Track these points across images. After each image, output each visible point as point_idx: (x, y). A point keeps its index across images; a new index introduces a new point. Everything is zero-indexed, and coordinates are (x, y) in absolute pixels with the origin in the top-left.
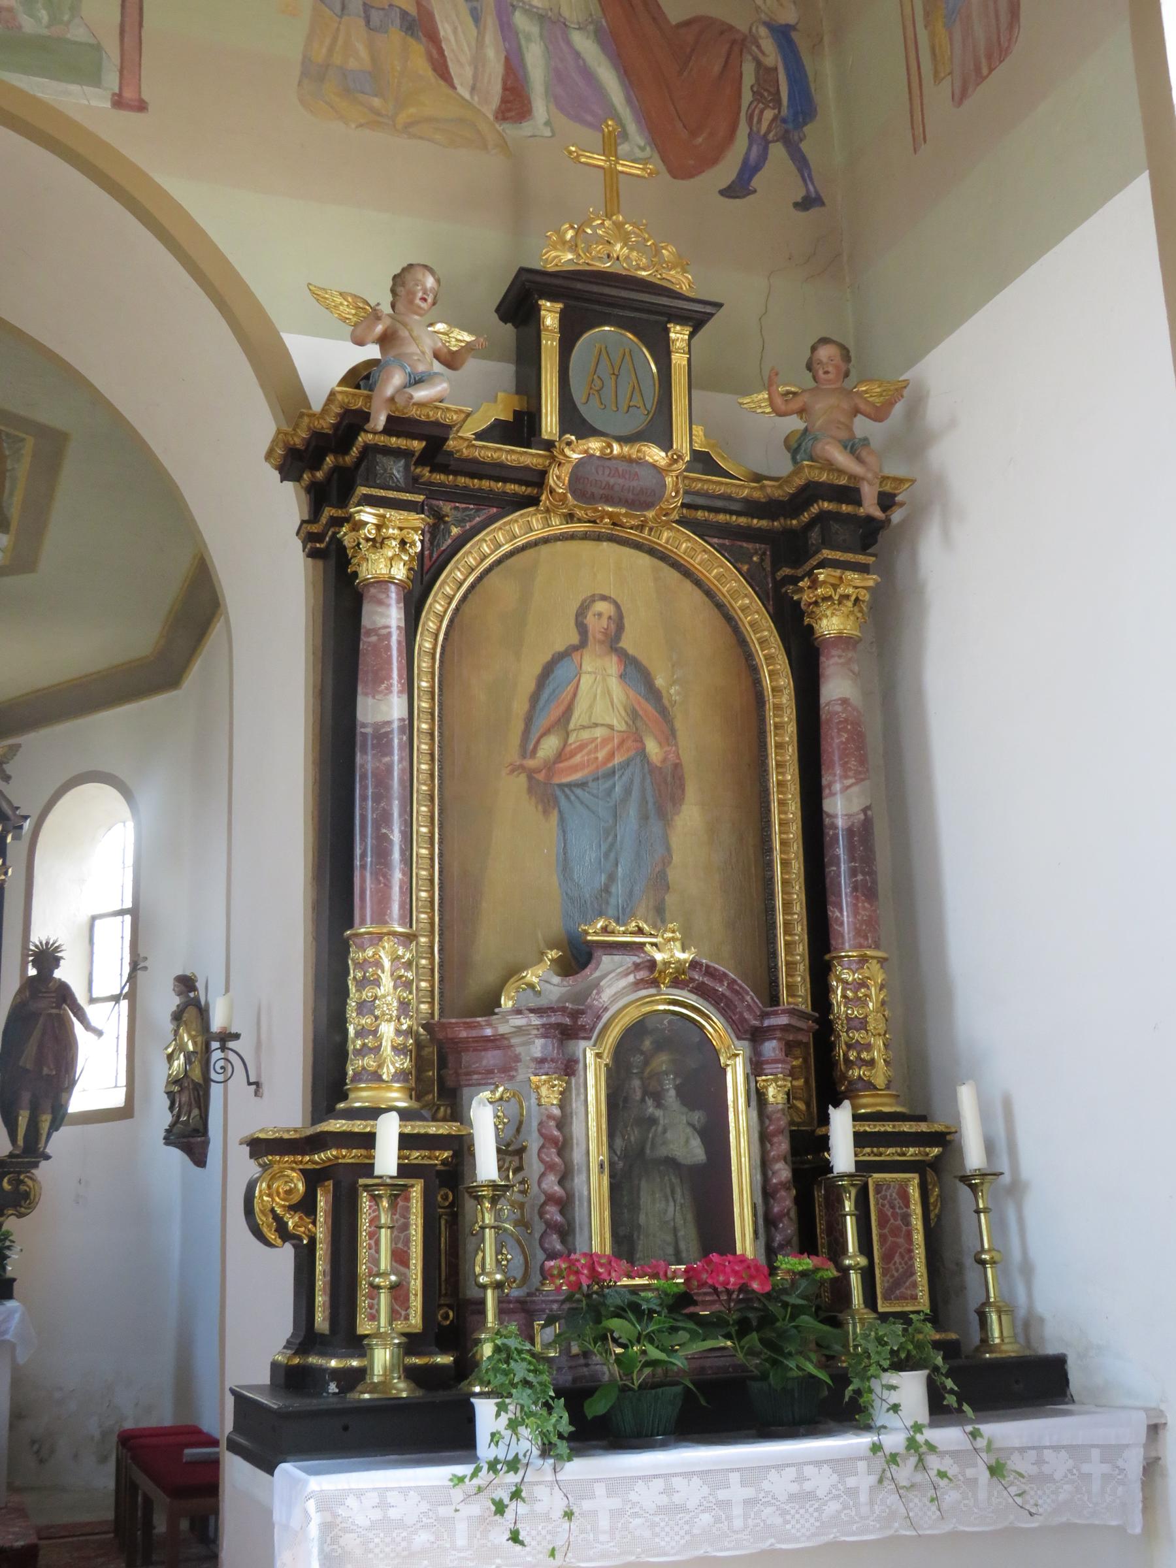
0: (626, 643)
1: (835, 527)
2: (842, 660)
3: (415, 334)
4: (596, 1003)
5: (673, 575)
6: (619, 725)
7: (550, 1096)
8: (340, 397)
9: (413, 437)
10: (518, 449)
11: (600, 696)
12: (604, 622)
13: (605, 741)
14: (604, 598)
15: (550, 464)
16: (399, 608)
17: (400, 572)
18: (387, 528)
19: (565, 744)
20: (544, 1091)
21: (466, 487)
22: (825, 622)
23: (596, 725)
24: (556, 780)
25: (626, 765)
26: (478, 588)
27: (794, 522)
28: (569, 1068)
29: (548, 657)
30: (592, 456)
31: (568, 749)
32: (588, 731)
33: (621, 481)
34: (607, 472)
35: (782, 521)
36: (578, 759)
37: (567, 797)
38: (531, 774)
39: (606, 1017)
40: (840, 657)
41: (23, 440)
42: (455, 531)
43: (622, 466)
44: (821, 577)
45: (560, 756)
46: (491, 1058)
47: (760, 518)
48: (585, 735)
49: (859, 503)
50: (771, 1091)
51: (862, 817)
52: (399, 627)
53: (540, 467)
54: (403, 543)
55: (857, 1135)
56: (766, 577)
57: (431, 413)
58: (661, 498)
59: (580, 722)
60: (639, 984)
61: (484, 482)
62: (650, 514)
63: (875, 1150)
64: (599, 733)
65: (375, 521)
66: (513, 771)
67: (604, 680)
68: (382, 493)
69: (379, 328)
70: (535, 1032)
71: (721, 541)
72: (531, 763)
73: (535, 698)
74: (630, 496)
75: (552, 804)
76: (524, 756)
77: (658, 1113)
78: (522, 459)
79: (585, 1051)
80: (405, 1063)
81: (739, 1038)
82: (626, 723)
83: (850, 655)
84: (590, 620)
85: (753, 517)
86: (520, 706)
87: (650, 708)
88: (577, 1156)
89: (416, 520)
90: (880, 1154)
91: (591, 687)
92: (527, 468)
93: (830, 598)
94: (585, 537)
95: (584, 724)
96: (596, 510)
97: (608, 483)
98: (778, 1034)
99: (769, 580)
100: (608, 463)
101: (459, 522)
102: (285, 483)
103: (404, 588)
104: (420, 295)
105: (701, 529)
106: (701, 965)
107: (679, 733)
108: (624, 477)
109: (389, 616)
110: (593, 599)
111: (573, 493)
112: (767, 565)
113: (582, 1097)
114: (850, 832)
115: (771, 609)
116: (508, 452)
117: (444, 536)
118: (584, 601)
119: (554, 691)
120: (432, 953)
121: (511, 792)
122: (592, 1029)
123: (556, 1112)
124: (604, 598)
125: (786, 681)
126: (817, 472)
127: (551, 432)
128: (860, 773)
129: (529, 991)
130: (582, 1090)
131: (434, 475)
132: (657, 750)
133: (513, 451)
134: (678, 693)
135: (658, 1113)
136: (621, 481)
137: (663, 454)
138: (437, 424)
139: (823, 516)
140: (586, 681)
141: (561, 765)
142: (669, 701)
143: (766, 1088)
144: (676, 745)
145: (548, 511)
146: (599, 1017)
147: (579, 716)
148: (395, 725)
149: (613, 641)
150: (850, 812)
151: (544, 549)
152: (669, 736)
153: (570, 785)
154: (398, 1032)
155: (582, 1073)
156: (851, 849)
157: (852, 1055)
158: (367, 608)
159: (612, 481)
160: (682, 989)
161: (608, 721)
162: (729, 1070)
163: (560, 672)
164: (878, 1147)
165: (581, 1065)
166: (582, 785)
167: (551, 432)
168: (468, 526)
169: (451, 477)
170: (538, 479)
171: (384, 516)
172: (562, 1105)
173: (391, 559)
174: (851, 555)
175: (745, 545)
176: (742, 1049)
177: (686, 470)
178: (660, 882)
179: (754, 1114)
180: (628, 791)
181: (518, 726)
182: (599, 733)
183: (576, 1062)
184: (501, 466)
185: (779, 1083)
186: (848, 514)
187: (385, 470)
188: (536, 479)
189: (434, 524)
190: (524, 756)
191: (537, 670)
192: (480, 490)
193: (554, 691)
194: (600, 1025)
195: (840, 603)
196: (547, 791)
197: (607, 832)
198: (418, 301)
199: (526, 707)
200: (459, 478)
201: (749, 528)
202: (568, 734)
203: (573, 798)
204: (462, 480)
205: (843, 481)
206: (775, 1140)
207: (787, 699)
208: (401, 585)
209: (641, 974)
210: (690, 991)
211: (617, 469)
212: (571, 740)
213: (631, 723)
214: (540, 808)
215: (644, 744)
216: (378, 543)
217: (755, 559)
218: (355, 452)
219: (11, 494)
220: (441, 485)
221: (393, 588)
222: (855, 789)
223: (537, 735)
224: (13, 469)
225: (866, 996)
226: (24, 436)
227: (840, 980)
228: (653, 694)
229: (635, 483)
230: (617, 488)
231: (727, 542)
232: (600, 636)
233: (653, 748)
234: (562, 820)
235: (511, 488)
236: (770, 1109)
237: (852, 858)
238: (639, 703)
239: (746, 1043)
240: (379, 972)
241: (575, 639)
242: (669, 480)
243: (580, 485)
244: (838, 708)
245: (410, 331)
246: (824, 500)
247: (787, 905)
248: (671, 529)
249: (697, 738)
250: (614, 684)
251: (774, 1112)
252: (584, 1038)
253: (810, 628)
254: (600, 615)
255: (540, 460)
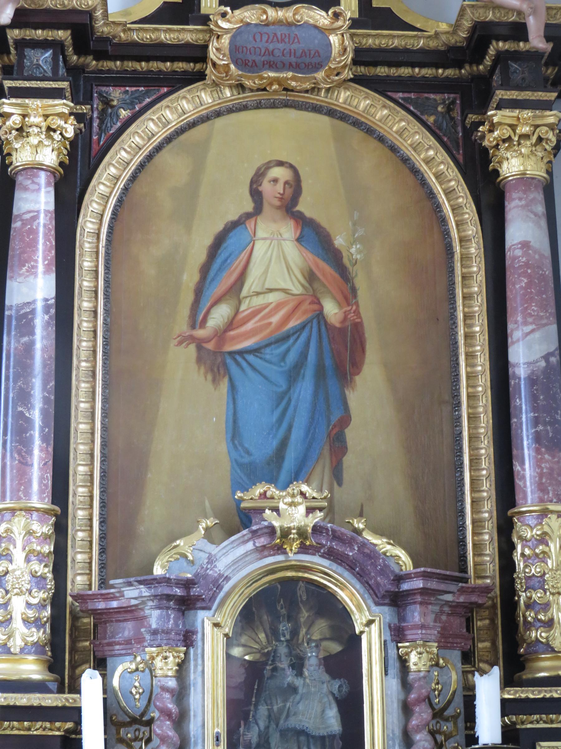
0: (301, 207)
1: (514, 66)
2: (523, 202)
4: (211, 572)
5: (357, 135)
6: (297, 289)
7: (165, 667)
10: (175, 27)
11: (275, 262)
12: (280, 188)
13: (279, 306)
14: (280, 164)
15: (210, 37)
17: (49, 157)
19: (237, 312)
20: (158, 663)
22: (505, 165)
23: (271, 290)
24: (229, 348)
25: (303, 327)
26: (150, 167)
27: (75, 58)
28: (188, 639)
29: (220, 227)
30: (248, 24)
31: (241, 316)
32: (261, 296)
33: (281, 46)
34: (265, 38)
35: (467, 67)
36: (250, 326)
37: (238, 364)
38: (200, 344)
39: (227, 587)
40: (520, 199)
42: (124, 113)
43: (280, 31)
44: (496, 119)
45: (231, 325)
46: (127, 630)
47: (445, 67)
48: (258, 301)
49: (526, 40)
50: (413, 658)
51: (543, 364)
53: (201, 42)
55: (504, 702)
56: (455, 126)
58: (328, 58)
59: (253, 289)
60: (262, 551)
61: (151, 64)
62: (320, 75)
63: (544, 716)
64: (272, 298)
66: (180, 343)
67: (280, 245)
68: (27, 84)
70: (150, 603)
71: (406, 95)
72: (200, 333)
73: (205, 270)
74: (293, 60)
75: (222, 372)
76: (193, 327)
77: (298, 682)
79: (203, 622)
80: (38, 635)
81: (377, 604)
82: (303, 286)
83: (532, 196)
84: (266, 187)
85: (437, 68)
86: (190, 278)
87: (328, 269)
88: (193, 727)
89: (62, 106)
90: (552, 722)
91: (266, 253)
92: (187, 45)
93: (509, 139)
94: (258, 106)
95: (258, 290)
96: (262, 78)
97: (267, 49)
98: (419, 598)
99: (459, 129)
100: (265, 29)
101: (130, 105)
103: (53, 173)
105: (380, 87)
106: (327, 529)
107: (359, 293)
108: (283, 40)
109: (37, 202)
110: (268, 166)
111: (236, 64)
112: (457, 114)
113: (200, 668)
114: (532, 381)
115: (460, 158)
117: (112, 119)
118: (259, 169)
119: (226, 260)
120: (91, 526)
121: (180, 365)
122: (212, 599)
123: (172, 683)
124: (280, 164)
125: (473, 229)
126: (481, 11)
128: (541, 318)
129: (183, 561)
130: (200, 662)
132: (336, 311)
133: (170, 30)
134: (359, 252)
135: (298, 682)
136: (281, 46)
137: (323, 13)
139: (502, 58)
140: (260, 248)
141: (232, 333)
142: (350, 260)
143: (407, 654)
144: (357, 304)
145: (215, 84)
146: (219, 587)
147: (252, 283)
148: (39, 305)
149: (289, 206)
150: (531, 360)
151: (219, 122)
152: (348, 295)
153: (241, 353)
154: (29, 605)
155: (200, 643)
156: (534, 398)
157: (530, 616)
158: (18, 195)
159: (271, 47)
160: (314, 554)
161: (283, 285)
162: (364, 638)
163: (232, 241)
164: (547, 714)
165: (199, 635)
166: (255, 351)
169: (118, 63)
170: (198, 54)
172: (182, 668)
173: (37, 146)
174: (530, 93)
175: (432, 96)
176: (384, 614)
177: (350, 28)
178: (338, 446)
179: (394, 683)
180: (304, 355)
181: (188, 298)
182: (272, 298)
183: (194, 633)
184: (161, 45)
185: (419, 650)
186: (507, 51)
187: (32, 62)
188: (199, 54)
190: (193, 327)
191: (208, 241)
193: (226, 260)
194: (222, 594)
195: (519, 144)
196: (217, 360)
197: (281, 397)
199: (196, 277)
200: (126, 63)
201: (436, 78)
202: (240, 302)
203: (244, 364)
204: (130, 65)
205: (513, 18)
206: (417, 709)
207: (476, 248)
208: (51, 171)
209: (262, 541)
210: (322, 556)
211: (275, 34)
212: (242, 308)
213: (307, 285)
214: (210, 377)
215: (319, 303)
217: (440, 109)
218: (488, 61)
220: (110, 71)
222: (537, 335)
223: (208, 305)
225: (544, 552)
227: (520, 538)
228: (334, 257)
229: (294, 46)
230: (277, 53)
231: (412, 96)
232: (277, 203)
233: (331, 310)
234: (233, 387)
235: (180, 66)
236: (411, 677)
237: (535, 409)
238: (317, 266)
239: (386, 609)
240: (11, 547)
241: (249, 206)
242: (334, 39)
243: (237, 54)
244: (518, 253)
246: (498, 40)
247: (475, 461)
248: (346, 89)
249: (380, 292)
250: (293, 252)
251: (415, 680)
252: (203, 608)
253: (496, 173)
254: (275, 181)
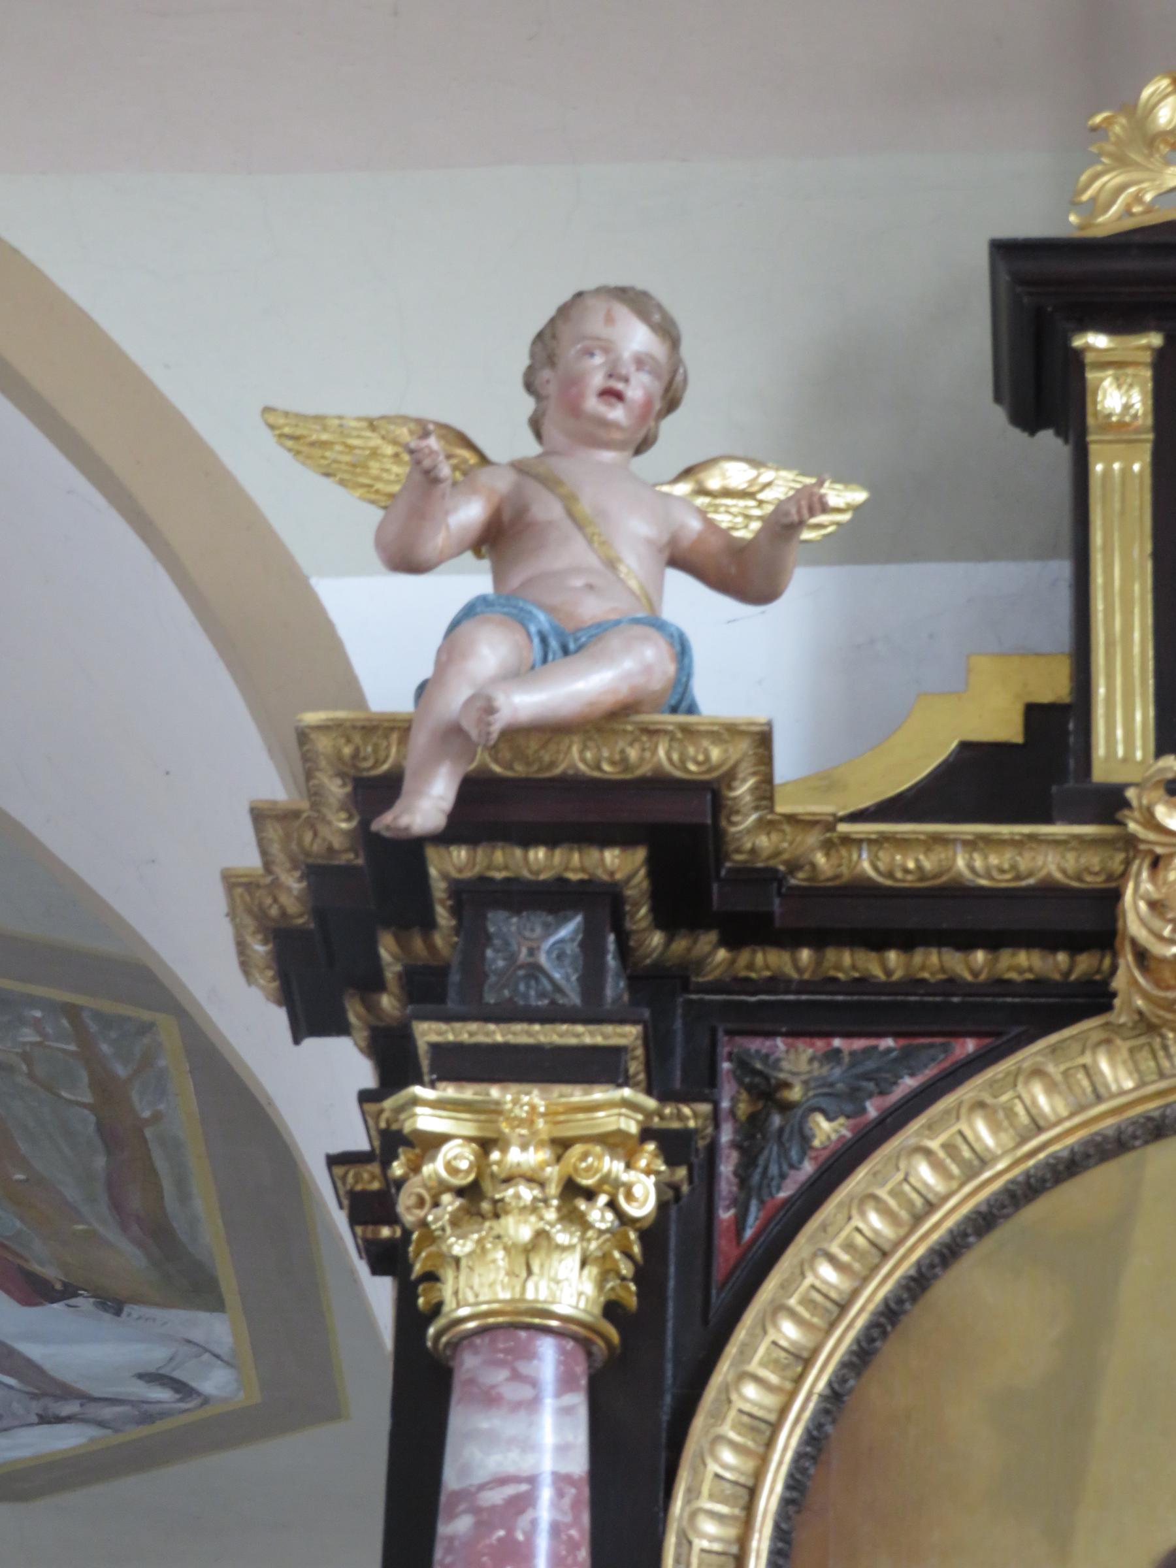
3: (585, 506)
8: (323, 744)
9: (603, 837)
15: (1128, 863)
16: (565, 1412)
17: (570, 1287)
18: (504, 1150)
21: (863, 983)
26: (919, 1318)
41: (146, 1028)
42: (826, 1130)
52: (561, 1480)
53: (1094, 881)
54: (574, 1191)
57: (633, 754)
61: (918, 957)
65: (469, 1129)
68: (496, 1034)
69: (470, 513)
78: (1024, 862)
92: (1048, 891)
102: (312, 1044)
103: (585, 1344)
104: (598, 380)
109: (528, 1445)
116: (972, 844)
117: (784, 1153)
127: (1128, 758)
131: (744, 957)
138: (660, 784)
158: (462, 1419)
167: (1128, 758)
168: (872, 1111)
169: (805, 954)
171: (493, 1110)
173: (529, 1250)
184: (956, 894)
187: (512, 958)
189: (753, 1118)
192: (913, 983)
198: (592, 404)
200: (831, 954)
204: (847, 962)
208: (573, 1334)
216: (476, 1197)
219: (184, 1197)
220: (775, 983)
221: (547, 1348)
224: (157, 1117)
226: (146, 1016)
235: (1022, 963)
245: (569, 502)
255: (1094, 860)
